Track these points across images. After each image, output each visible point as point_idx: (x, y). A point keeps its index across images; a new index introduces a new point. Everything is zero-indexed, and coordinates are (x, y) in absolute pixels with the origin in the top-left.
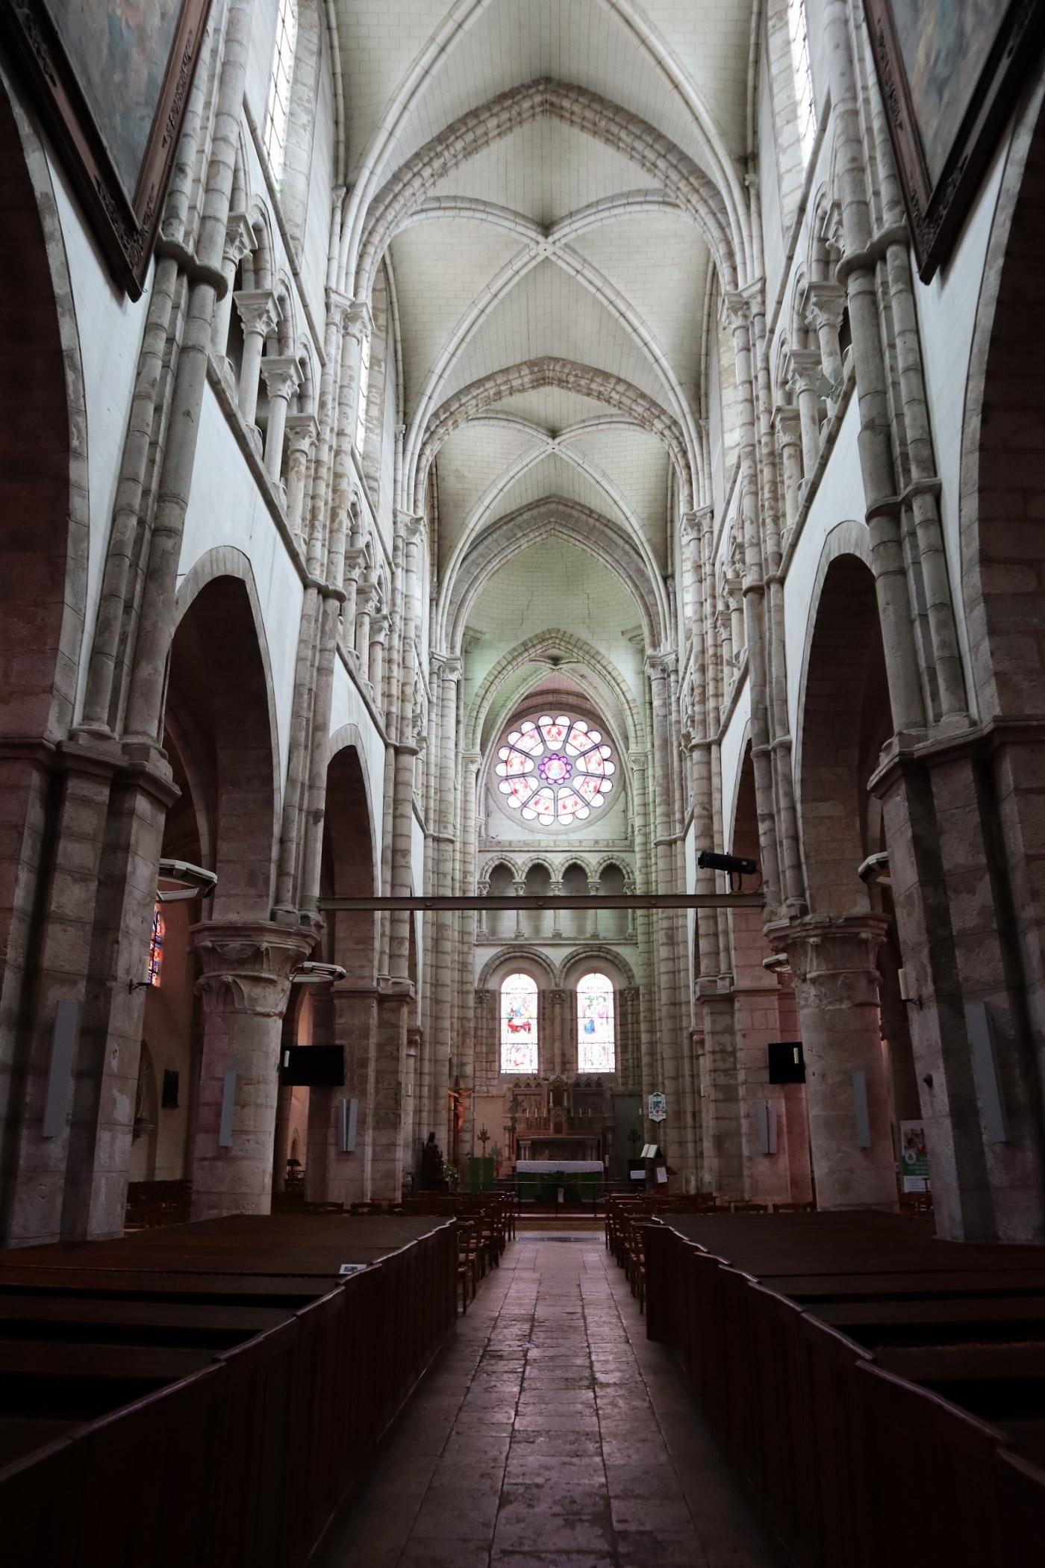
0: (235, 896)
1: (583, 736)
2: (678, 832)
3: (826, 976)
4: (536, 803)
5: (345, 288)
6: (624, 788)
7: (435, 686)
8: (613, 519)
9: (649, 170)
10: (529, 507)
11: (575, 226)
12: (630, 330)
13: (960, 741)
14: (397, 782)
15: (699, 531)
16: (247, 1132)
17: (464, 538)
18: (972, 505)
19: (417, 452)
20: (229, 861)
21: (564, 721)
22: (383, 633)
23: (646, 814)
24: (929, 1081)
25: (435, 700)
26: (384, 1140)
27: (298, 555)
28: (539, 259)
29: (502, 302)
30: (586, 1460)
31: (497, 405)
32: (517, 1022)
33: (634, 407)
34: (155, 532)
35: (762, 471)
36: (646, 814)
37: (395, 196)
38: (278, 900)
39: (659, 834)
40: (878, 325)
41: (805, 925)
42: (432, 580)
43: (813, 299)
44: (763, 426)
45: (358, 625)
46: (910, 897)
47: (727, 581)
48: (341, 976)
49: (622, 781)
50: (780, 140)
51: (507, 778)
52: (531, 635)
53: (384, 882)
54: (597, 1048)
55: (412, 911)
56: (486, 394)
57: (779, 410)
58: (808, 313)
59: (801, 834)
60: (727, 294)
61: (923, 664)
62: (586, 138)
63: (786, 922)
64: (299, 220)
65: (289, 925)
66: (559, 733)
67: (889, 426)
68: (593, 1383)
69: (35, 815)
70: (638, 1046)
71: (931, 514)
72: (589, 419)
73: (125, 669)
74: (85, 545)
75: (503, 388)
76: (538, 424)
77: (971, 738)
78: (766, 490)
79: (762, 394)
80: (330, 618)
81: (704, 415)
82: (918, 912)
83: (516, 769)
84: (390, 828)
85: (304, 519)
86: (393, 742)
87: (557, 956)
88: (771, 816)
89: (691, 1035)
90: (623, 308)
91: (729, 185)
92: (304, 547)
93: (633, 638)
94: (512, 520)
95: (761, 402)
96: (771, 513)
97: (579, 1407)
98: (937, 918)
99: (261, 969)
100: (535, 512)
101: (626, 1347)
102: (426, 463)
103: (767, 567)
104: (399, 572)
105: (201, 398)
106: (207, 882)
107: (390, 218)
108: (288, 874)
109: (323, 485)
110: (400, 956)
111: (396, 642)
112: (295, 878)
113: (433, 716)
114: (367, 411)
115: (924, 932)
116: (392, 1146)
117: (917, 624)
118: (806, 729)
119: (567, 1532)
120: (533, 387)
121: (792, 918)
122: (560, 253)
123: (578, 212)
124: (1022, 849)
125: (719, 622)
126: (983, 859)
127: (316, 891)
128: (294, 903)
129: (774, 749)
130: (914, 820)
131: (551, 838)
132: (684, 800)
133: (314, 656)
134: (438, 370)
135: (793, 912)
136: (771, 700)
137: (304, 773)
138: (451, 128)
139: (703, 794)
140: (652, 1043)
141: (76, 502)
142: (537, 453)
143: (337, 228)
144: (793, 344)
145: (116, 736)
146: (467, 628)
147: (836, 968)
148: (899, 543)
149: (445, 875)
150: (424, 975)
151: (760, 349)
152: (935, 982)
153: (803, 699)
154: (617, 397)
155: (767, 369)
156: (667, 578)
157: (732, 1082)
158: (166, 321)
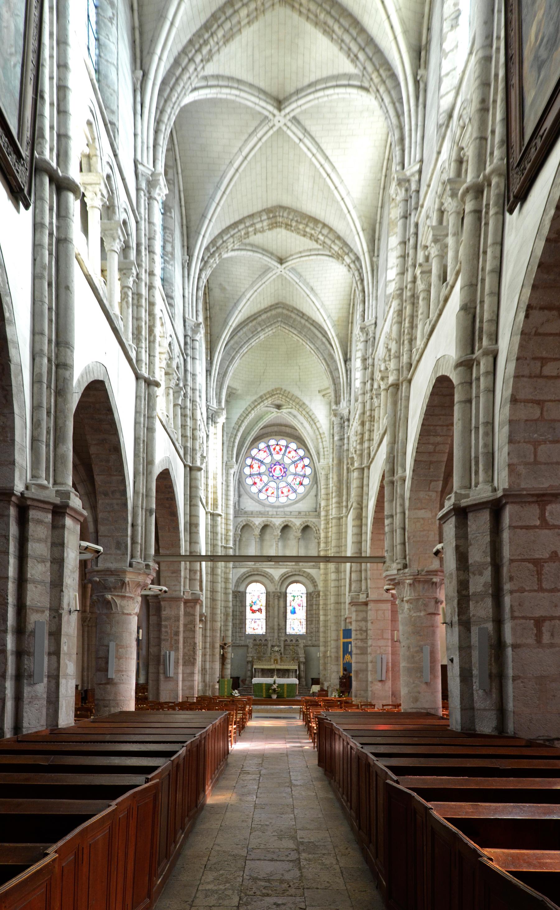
0: (110, 554)
4: (267, 490)
5: (192, 320)
6: (316, 483)
8: (317, 320)
9: (352, 61)
11: (300, 102)
12: (332, 187)
13: (485, 500)
18: (512, 366)
20: (105, 536)
21: (283, 442)
23: (327, 500)
26: (188, 671)
27: (132, 359)
28: (275, 129)
29: (249, 163)
31: (247, 241)
32: (255, 608)
33: (333, 246)
34: (57, 366)
35: (406, 308)
36: (327, 500)
37: (177, 80)
38: (132, 557)
42: (207, 359)
46: (451, 574)
47: (380, 371)
48: (165, 592)
50: (445, 46)
52: (265, 392)
53: (185, 541)
54: (297, 623)
55: (200, 562)
57: (420, 265)
59: (407, 526)
61: (473, 455)
62: (309, 27)
63: (395, 572)
66: (281, 450)
67: (475, 308)
70: (319, 621)
71: (491, 369)
72: (304, 251)
75: (250, 229)
77: (491, 499)
79: (411, 252)
81: (376, 254)
83: (255, 470)
85: (133, 334)
88: (392, 516)
89: (346, 619)
90: (329, 170)
91: (406, 79)
92: (134, 352)
94: (255, 319)
95: (410, 259)
97: (284, 795)
100: (269, 314)
102: (203, 283)
103: (402, 371)
104: (189, 359)
106: (98, 552)
107: (174, 99)
109: (143, 311)
111: (189, 404)
112: (141, 545)
114: (164, 247)
115: (456, 592)
116: (192, 673)
120: (269, 229)
121: (398, 570)
122: (289, 124)
123: (302, 90)
126: (489, 559)
127: (153, 552)
128: (141, 558)
130: (457, 537)
131: (274, 510)
132: (348, 494)
136: (397, 452)
138: (214, 17)
140: (326, 621)
146: (229, 387)
152: (459, 616)
153: (414, 454)
156: (347, 360)
157: (365, 645)
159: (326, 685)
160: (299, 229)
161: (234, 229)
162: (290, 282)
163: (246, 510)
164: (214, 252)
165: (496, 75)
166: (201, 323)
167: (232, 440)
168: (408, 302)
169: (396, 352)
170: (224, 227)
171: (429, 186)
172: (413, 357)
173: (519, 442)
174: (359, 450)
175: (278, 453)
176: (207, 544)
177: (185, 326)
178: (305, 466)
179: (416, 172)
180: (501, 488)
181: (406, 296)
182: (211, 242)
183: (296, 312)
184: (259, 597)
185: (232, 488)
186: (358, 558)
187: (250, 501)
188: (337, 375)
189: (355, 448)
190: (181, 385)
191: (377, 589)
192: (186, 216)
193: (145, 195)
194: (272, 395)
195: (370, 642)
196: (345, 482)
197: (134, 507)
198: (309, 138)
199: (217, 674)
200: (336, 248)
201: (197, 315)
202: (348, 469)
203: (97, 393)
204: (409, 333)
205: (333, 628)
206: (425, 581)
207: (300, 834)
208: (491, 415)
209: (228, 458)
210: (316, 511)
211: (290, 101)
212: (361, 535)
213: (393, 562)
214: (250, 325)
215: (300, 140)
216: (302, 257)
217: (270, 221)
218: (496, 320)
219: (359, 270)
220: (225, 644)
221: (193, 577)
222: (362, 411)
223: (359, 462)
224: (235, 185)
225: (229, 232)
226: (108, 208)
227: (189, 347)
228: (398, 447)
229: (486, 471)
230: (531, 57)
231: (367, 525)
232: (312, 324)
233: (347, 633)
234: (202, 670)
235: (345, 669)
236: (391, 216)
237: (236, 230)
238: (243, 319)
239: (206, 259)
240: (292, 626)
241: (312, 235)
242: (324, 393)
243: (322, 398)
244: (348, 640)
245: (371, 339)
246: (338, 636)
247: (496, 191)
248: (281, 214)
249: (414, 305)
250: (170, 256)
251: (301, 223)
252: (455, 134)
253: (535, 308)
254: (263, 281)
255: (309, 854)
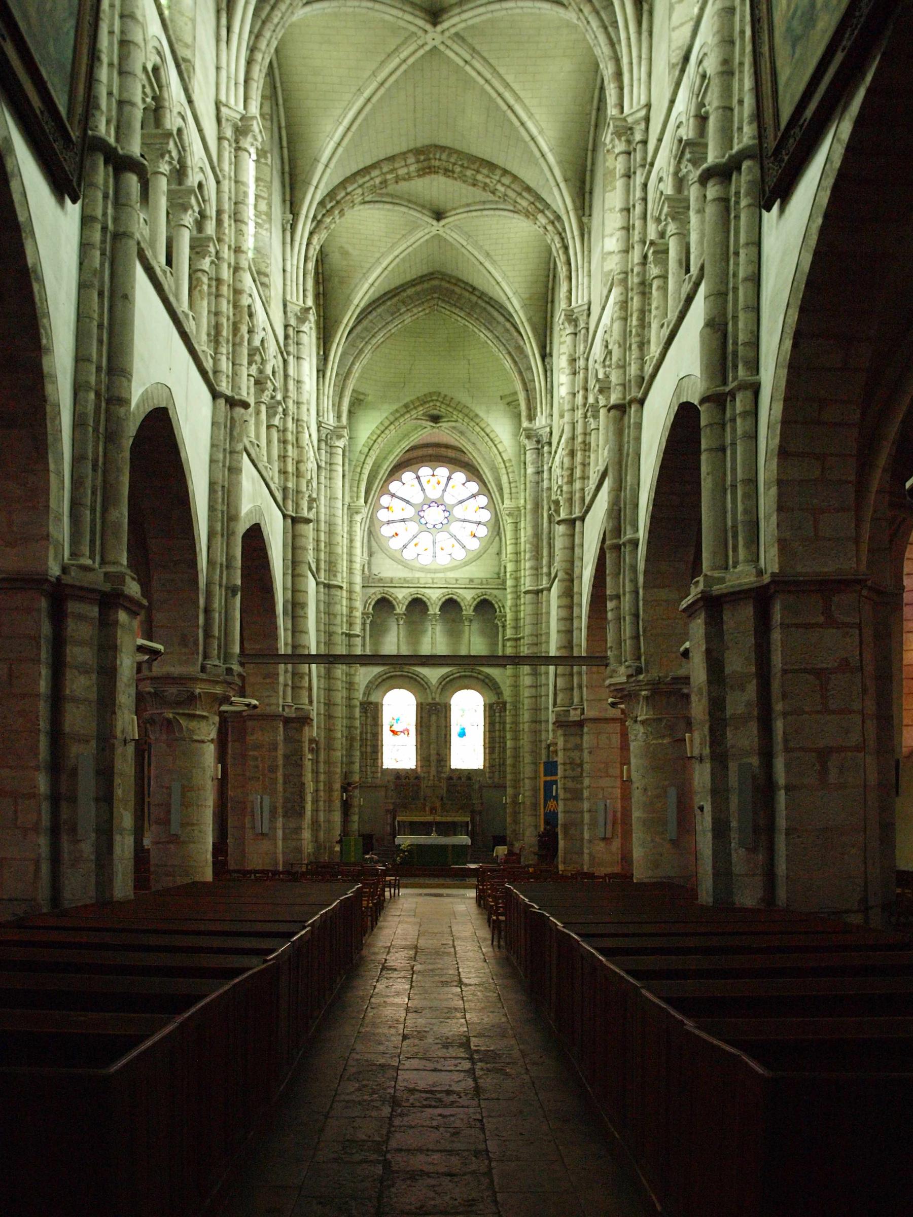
1: (460, 485)
2: (545, 583)
3: (654, 720)
5: (235, 106)
6: (499, 534)
7: (323, 452)
8: (495, 297)
10: (413, 283)
12: (517, 124)
15: (576, 326)
16: (193, 825)
17: (349, 313)
18: (779, 407)
22: (278, 417)
23: (517, 561)
24: (701, 809)
25: (323, 465)
26: (292, 825)
27: (207, 372)
28: (427, 48)
30: (455, 1021)
33: (519, 200)
34: (109, 401)
35: (632, 299)
38: (206, 656)
39: (527, 584)
40: (728, 232)
41: (639, 681)
42: (318, 354)
43: (688, 156)
44: (636, 256)
45: (258, 413)
47: (598, 380)
48: (255, 707)
52: (412, 398)
53: (285, 630)
56: (372, 180)
57: (652, 243)
58: (682, 166)
60: (613, 118)
61: (729, 523)
63: (624, 679)
64: (189, 40)
65: (219, 676)
67: (726, 324)
68: (460, 983)
69: (46, 629)
73: (98, 515)
74: (57, 422)
75: (389, 177)
76: (423, 207)
78: (634, 318)
79: (638, 224)
80: (237, 424)
81: (587, 213)
82: (705, 701)
84: (289, 585)
85: (209, 335)
86: (290, 513)
88: (618, 597)
89: (549, 746)
90: (512, 101)
92: (211, 361)
93: (511, 403)
94: (395, 296)
95: (636, 232)
96: (637, 339)
97: (450, 996)
98: (717, 705)
99: (195, 708)
100: (419, 288)
101: (481, 964)
103: (630, 387)
104: (291, 360)
105: (135, 272)
107: (276, 20)
108: (214, 636)
110: (301, 688)
111: (290, 425)
112: (219, 639)
113: (322, 480)
114: (256, 206)
116: (298, 830)
117: (729, 491)
118: (651, 532)
119: (445, 1050)
120: (419, 176)
121: (629, 676)
122: (449, 43)
124: (780, 665)
125: (589, 414)
126: (753, 669)
127: (237, 649)
128: (219, 658)
129: (624, 544)
131: (429, 575)
132: (551, 556)
133: (225, 457)
134: (324, 159)
135: (630, 671)
137: (222, 555)
139: (566, 561)
140: (516, 749)
141: (49, 389)
142: (422, 234)
143: (224, 32)
144: (668, 188)
145: (97, 565)
147: (661, 714)
148: (723, 426)
149: (335, 615)
150: (318, 696)
151: (639, 179)
152: (711, 747)
153: (651, 508)
154: (502, 189)
155: (645, 199)
157: (579, 786)
158: (99, 213)
160: (465, 176)
161: (364, 177)
162: (451, 245)
163: (382, 575)
164: (332, 207)
165: (742, 32)
166: (310, 308)
167: (359, 470)
168: (635, 291)
169: (620, 360)
170: (348, 174)
172: (646, 368)
174: (567, 493)
176: (318, 631)
177: (285, 313)
180: (769, 571)
181: (632, 282)
182: (328, 195)
183: (463, 285)
185: (358, 544)
186: (567, 660)
187: (388, 561)
188: (530, 378)
189: (560, 487)
190: (279, 397)
191: (594, 703)
192: (290, 160)
193: (230, 145)
194: (425, 403)
195: (586, 782)
196: (545, 537)
197: (209, 584)
198: (479, 59)
199: (337, 832)
200: (524, 203)
201: (305, 296)
202: (550, 517)
203: (160, 424)
204: (638, 335)
205: (528, 759)
206: (670, 694)
207: (474, 1041)
208: (754, 468)
209: (351, 497)
210: (500, 579)
211: (450, 14)
212: (572, 620)
213: (621, 663)
214: (389, 303)
215: (466, 62)
216: (471, 211)
217: (420, 165)
218: (755, 343)
219: (560, 234)
220: (349, 784)
221: (298, 684)
222: (570, 435)
223: (568, 511)
224: (365, 119)
225: (355, 181)
226: (178, 171)
227: (291, 342)
228: (625, 496)
229: (747, 546)
230: (783, 29)
231: (580, 605)
232: (488, 303)
233: (551, 768)
234: (313, 823)
235: (547, 822)
236: (607, 164)
237: (367, 178)
238: (377, 295)
239: (319, 218)
241: (486, 184)
242: (510, 399)
243: (507, 408)
244: (553, 778)
245: (583, 331)
246: (536, 771)
247: (749, 178)
248: (438, 156)
249: (645, 294)
251: (467, 168)
254: (409, 243)
255: (487, 1063)
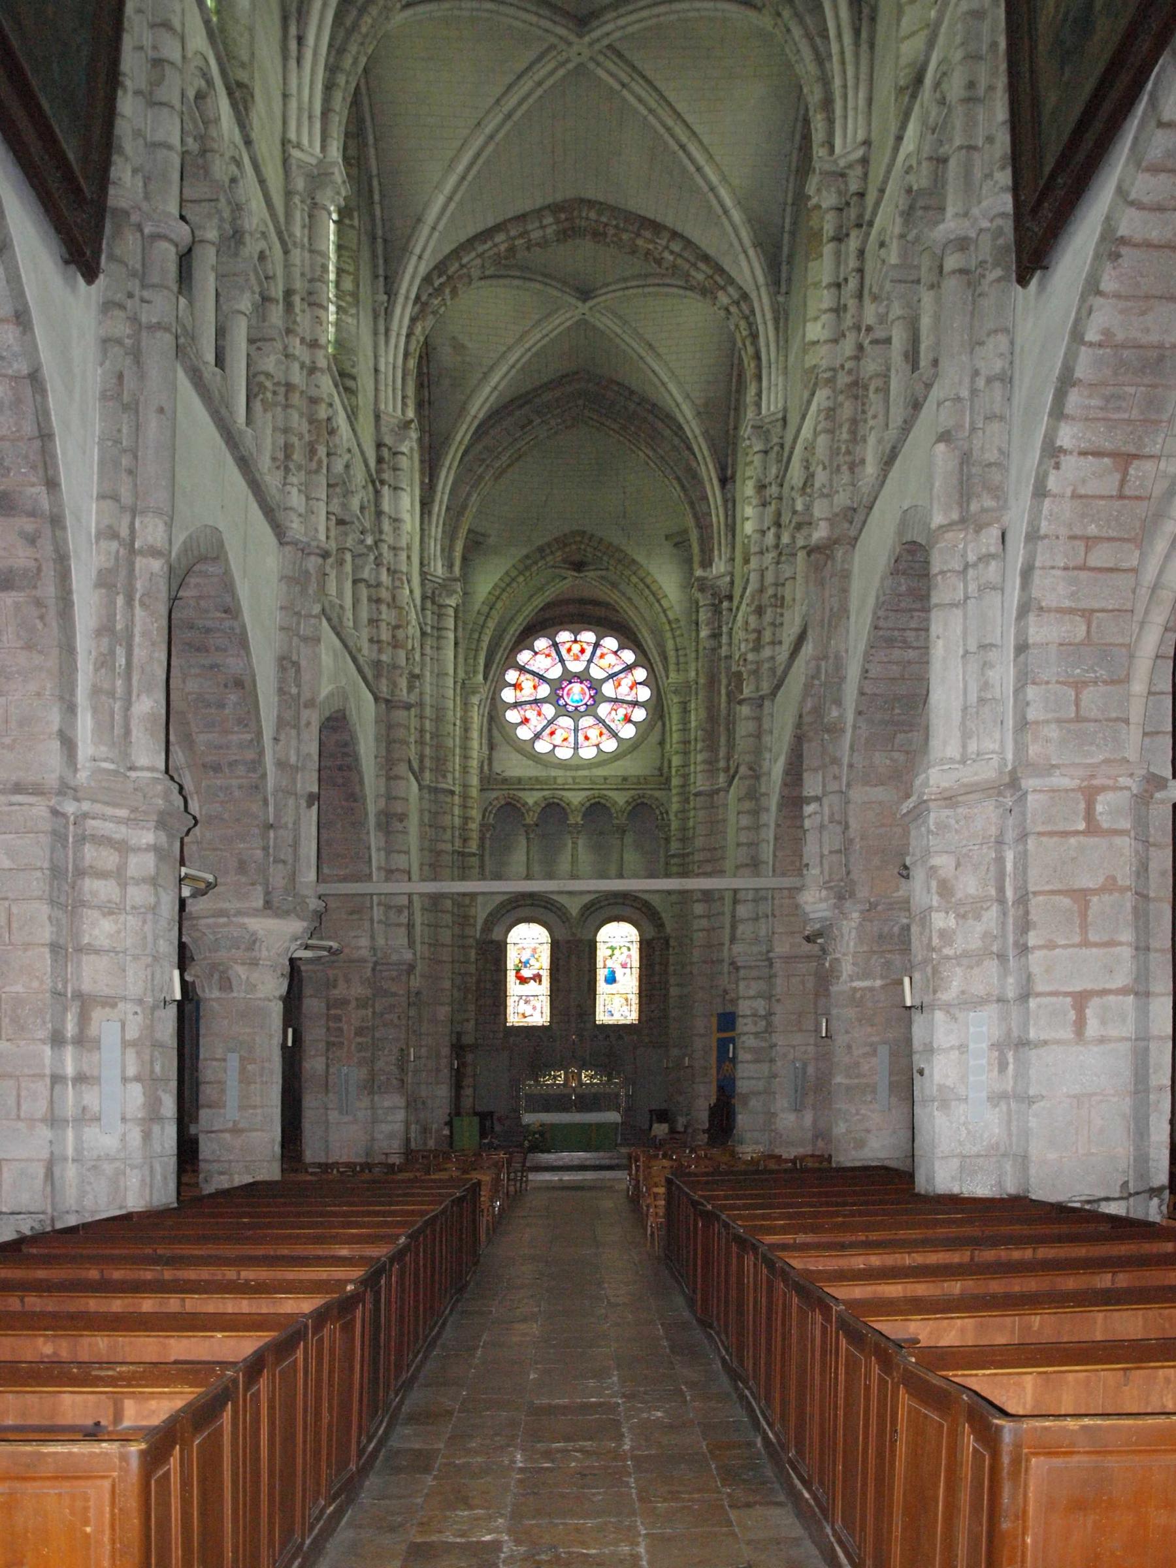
1: (612, 655)
4: (552, 733)
6: (662, 717)
12: (692, 169)
14: (389, 738)
15: (767, 440)
19: (404, 331)
21: (588, 637)
23: (686, 753)
28: (570, 66)
32: (526, 973)
33: (693, 273)
36: (686, 753)
42: (422, 483)
47: (795, 512)
49: (657, 707)
51: (516, 705)
54: (618, 1001)
66: (583, 651)
76: (565, 283)
83: (527, 693)
85: (274, 459)
87: (574, 907)
93: (679, 541)
104: (385, 490)
107: (364, 30)
113: (428, 650)
122: (601, 58)
131: (569, 773)
159: (681, 1121)
161: (485, 242)
163: (507, 774)
166: (412, 421)
167: (476, 636)
171: (882, 191)
173: (1047, 683)
175: (577, 658)
178: (636, 684)
179: (857, 161)
182: (436, 267)
184: (534, 950)
187: (515, 757)
201: (404, 404)
209: (466, 673)
210: (662, 777)
237: (489, 244)
239: (424, 298)
240: (609, 1007)
250: (348, 298)
252: (928, 113)
253: (1071, 453)
